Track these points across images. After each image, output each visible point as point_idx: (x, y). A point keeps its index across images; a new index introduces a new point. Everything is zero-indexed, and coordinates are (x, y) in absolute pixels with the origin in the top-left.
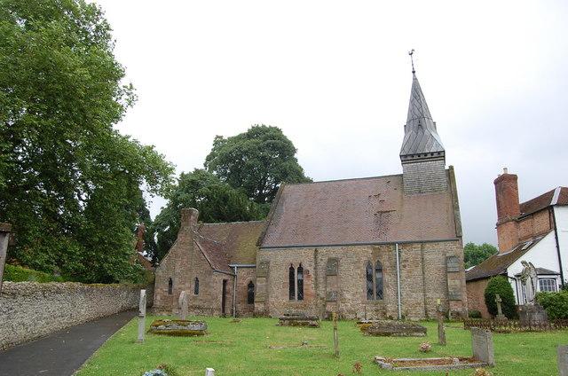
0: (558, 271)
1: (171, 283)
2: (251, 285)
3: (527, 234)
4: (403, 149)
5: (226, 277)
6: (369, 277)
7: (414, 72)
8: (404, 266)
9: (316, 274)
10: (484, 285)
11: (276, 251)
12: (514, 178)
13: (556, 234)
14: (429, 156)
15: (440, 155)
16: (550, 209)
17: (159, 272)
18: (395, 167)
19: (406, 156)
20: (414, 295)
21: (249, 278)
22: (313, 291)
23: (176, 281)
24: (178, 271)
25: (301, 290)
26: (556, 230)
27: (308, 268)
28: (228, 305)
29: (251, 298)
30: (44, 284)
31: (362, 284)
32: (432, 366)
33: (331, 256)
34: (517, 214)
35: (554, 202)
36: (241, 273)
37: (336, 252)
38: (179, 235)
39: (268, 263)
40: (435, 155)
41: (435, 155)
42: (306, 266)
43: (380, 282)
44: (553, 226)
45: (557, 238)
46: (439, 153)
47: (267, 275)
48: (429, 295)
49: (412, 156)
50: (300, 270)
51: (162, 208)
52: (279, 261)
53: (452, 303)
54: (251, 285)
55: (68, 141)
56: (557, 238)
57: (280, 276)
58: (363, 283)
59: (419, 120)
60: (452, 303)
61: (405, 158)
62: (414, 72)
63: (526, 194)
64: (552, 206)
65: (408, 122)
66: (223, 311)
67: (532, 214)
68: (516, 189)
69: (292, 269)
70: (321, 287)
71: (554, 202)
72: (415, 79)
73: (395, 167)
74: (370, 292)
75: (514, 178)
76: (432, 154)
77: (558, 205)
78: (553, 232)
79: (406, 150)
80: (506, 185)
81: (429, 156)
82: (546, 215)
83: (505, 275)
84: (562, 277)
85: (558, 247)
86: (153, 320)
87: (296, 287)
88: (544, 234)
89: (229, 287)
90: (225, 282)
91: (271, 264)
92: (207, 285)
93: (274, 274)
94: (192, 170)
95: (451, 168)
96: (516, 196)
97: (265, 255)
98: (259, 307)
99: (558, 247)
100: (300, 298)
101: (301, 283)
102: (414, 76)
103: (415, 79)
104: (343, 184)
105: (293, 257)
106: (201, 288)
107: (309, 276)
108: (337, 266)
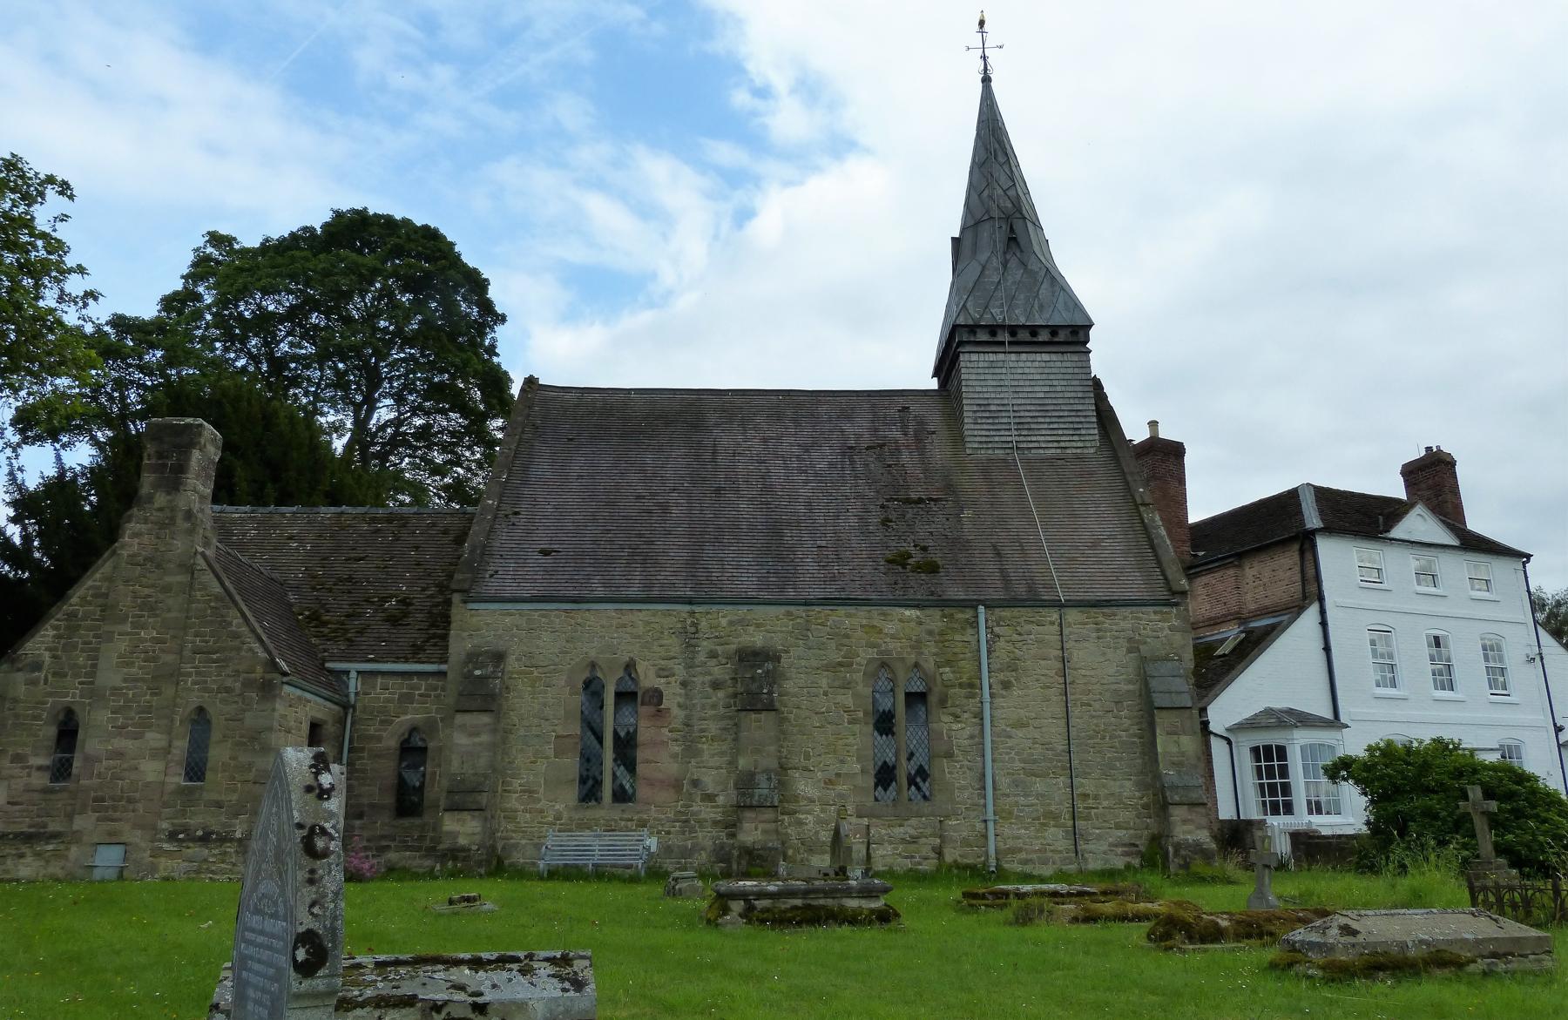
0: (1328, 714)
3: (1219, 610)
8: (1006, 685)
13: (1323, 612)
15: (1073, 335)
20: (1039, 785)
22: (671, 768)
24: (110, 676)
26: (1321, 599)
27: (659, 683)
31: (858, 748)
32: (462, 956)
38: (131, 527)
39: (499, 657)
44: (1311, 592)
45: (1324, 624)
48: (1086, 785)
51: (502, 319)
53: (1177, 813)
56: (1324, 624)
57: (543, 709)
59: (997, 218)
74: (885, 776)
88: (1297, 609)
91: (512, 663)
94: (327, 217)
96: (1178, 501)
104: (589, 397)
106: (218, 754)
107: (660, 713)
108: (773, 678)
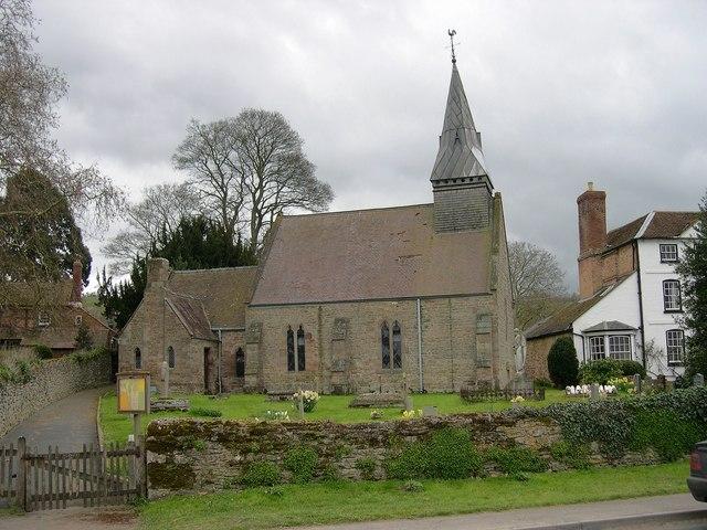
1: (138, 354)
2: (240, 353)
4: (434, 172)
5: (207, 345)
6: (385, 341)
7: (454, 61)
9: (320, 339)
10: (551, 342)
11: (270, 310)
12: (601, 197)
14: (467, 181)
16: (634, 243)
17: (122, 341)
18: (424, 194)
19: (438, 182)
21: (239, 344)
23: (145, 352)
24: (147, 338)
25: (291, 357)
28: (212, 380)
29: (240, 370)
30: (285, 414)
33: (338, 316)
34: (605, 246)
35: (640, 234)
36: (226, 339)
37: (343, 311)
39: (261, 325)
40: (475, 180)
41: (475, 180)
42: (307, 329)
43: (398, 346)
45: (639, 282)
46: (480, 177)
47: (259, 341)
49: (446, 181)
50: (301, 334)
52: (275, 325)
54: (240, 353)
55: (71, 277)
56: (639, 282)
57: (276, 340)
58: (378, 347)
60: (480, 371)
61: (439, 183)
62: (454, 61)
63: (615, 219)
64: (636, 240)
65: (444, 132)
66: (206, 387)
67: (617, 248)
68: (604, 211)
69: (290, 334)
70: (326, 355)
71: (640, 234)
72: (455, 72)
73: (424, 194)
74: (386, 360)
75: (601, 197)
76: (471, 179)
77: (643, 238)
78: (635, 276)
79: (439, 171)
80: (591, 204)
81: (467, 181)
82: (629, 251)
83: (571, 331)
84: (642, 333)
85: (640, 293)
86: (676, 277)
87: (296, 359)
88: (627, 276)
89: (212, 356)
90: (207, 351)
91: (265, 327)
92: (185, 355)
93: (268, 338)
95: (498, 195)
96: (602, 222)
97: (254, 315)
98: (251, 381)
99: (640, 293)
100: (302, 368)
101: (302, 350)
102: (455, 67)
103: (455, 72)
105: (293, 318)
106: (177, 359)
108: (347, 328)
